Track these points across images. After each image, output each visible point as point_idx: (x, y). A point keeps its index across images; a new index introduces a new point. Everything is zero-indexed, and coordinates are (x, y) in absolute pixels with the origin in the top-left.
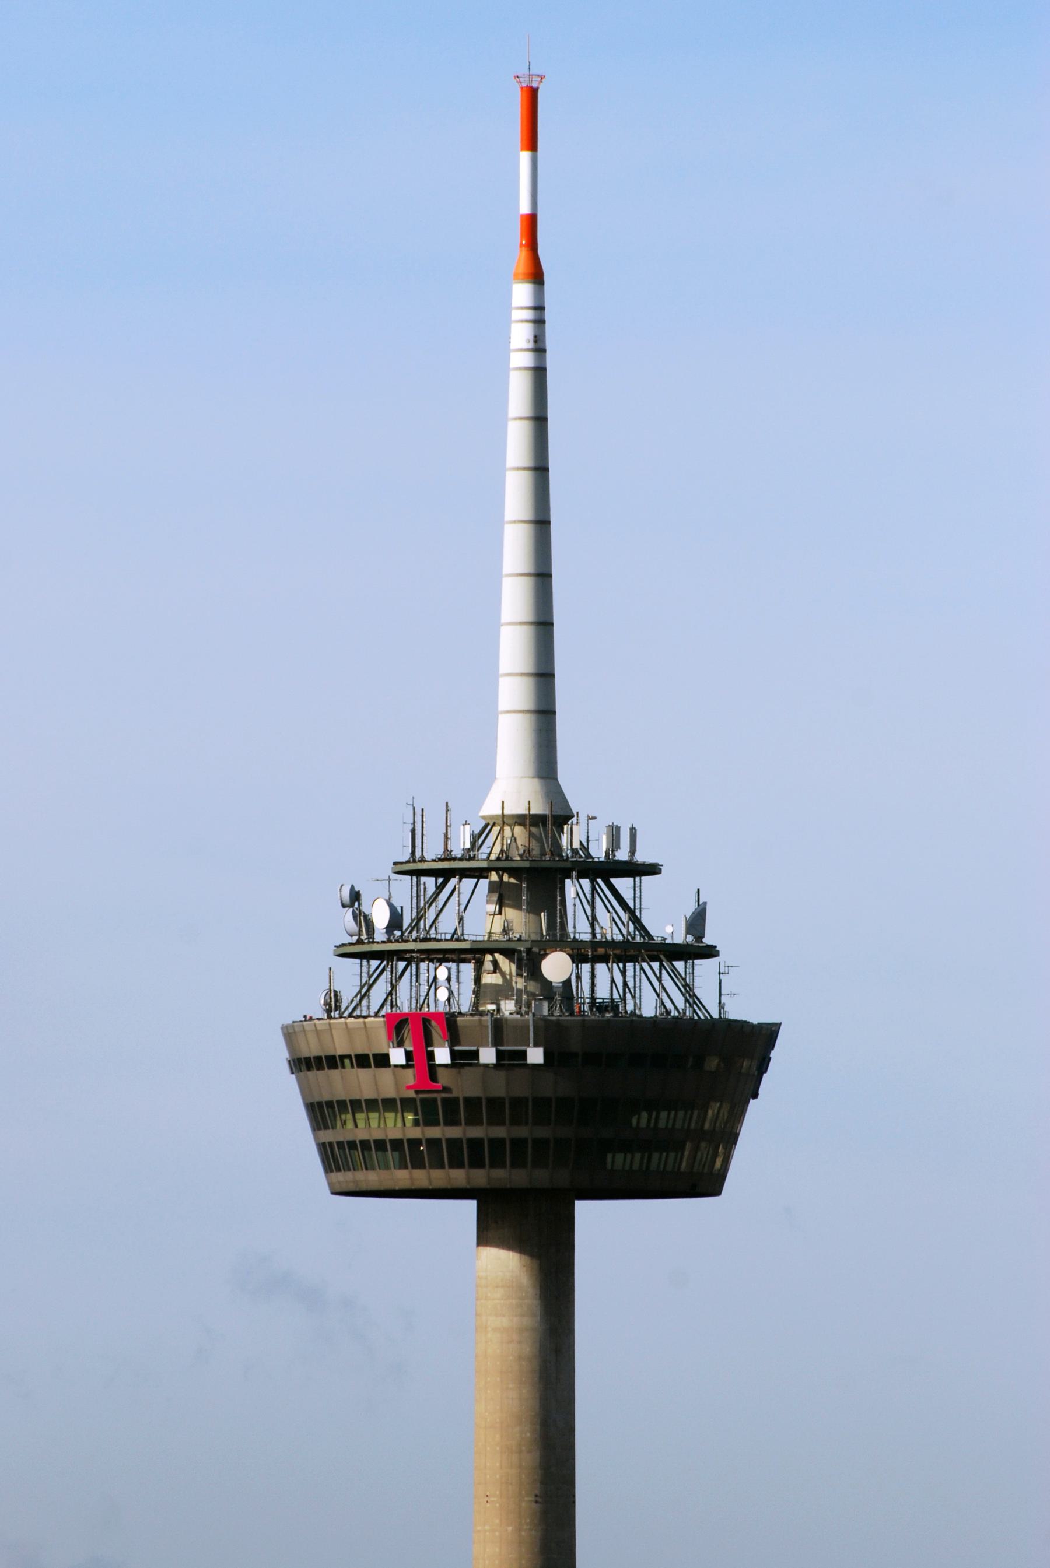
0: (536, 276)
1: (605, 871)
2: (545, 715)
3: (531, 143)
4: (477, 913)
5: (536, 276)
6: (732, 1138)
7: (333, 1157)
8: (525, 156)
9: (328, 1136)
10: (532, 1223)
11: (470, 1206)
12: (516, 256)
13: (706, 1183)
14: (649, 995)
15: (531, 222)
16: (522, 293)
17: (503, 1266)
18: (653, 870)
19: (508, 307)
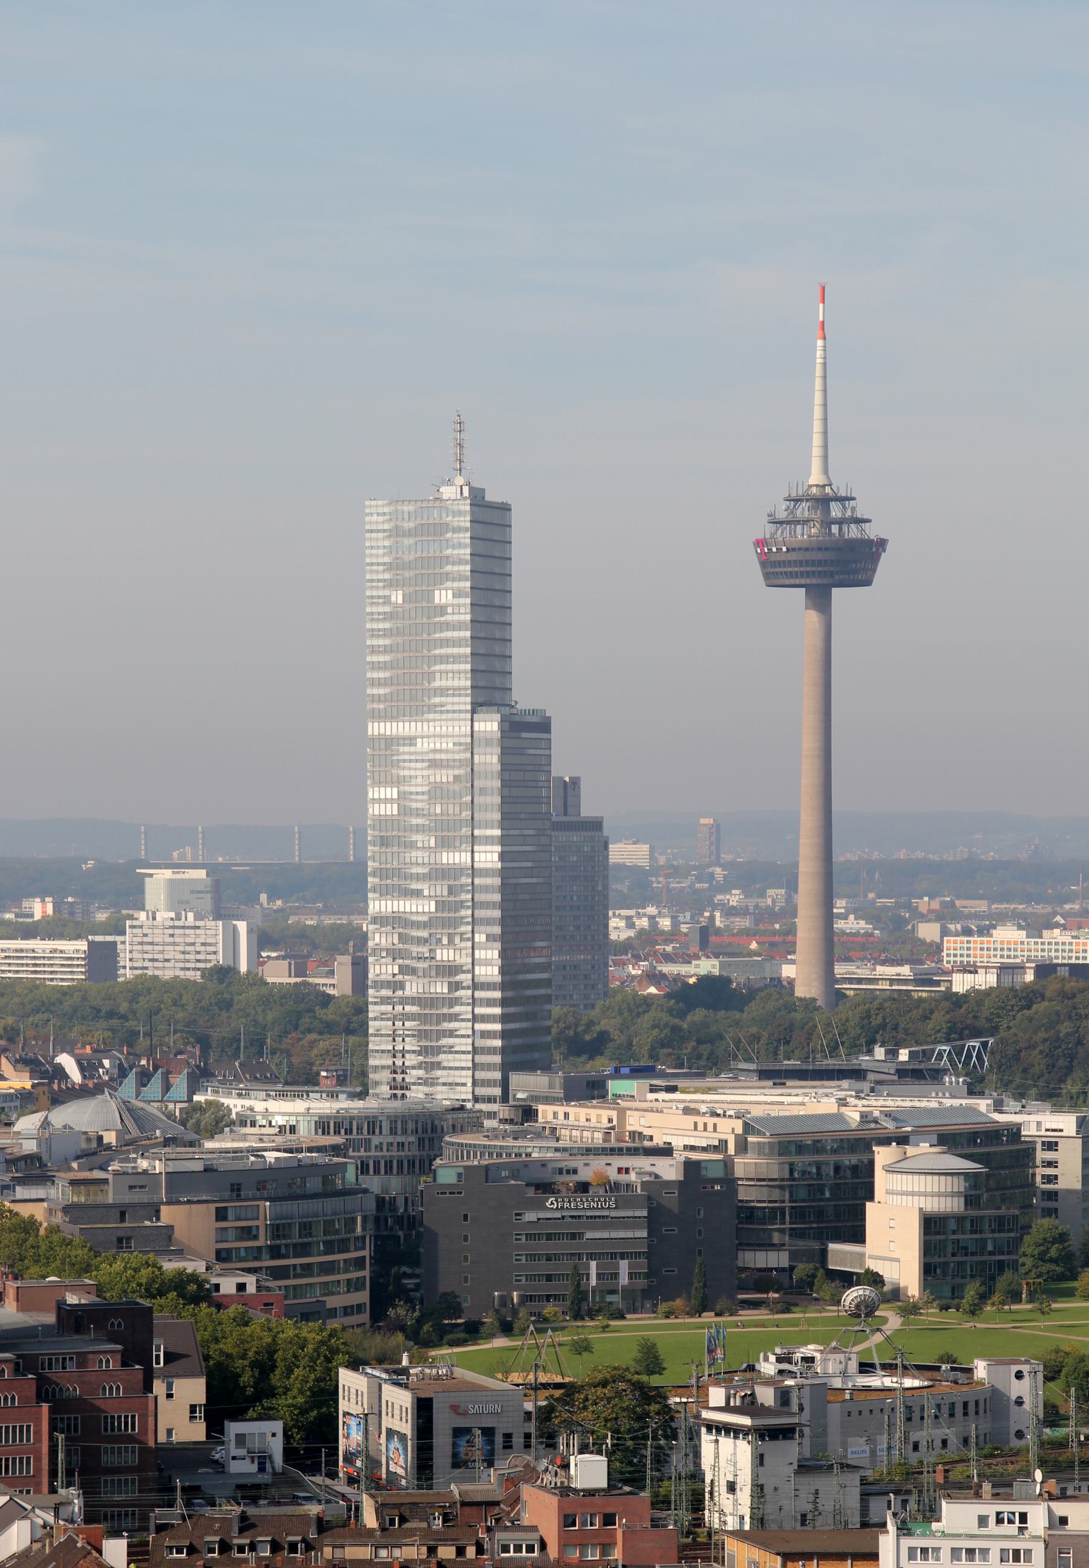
0: (824, 338)
1: (842, 500)
2: (825, 457)
3: (823, 302)
4: (803, 510)
5: (824, 338)
6: (874, 571)
7: (767, 576)
8: (821, 305)
9: (930, 1260)
10: (820, 599)
11: (804, 590)
12: (819, 333)
13: (868, 582)
14: (853, 532)
15: (823, 322)
16: (820, 343)
17: (813, 617)
18: (869, 521)
19: (816, 346)
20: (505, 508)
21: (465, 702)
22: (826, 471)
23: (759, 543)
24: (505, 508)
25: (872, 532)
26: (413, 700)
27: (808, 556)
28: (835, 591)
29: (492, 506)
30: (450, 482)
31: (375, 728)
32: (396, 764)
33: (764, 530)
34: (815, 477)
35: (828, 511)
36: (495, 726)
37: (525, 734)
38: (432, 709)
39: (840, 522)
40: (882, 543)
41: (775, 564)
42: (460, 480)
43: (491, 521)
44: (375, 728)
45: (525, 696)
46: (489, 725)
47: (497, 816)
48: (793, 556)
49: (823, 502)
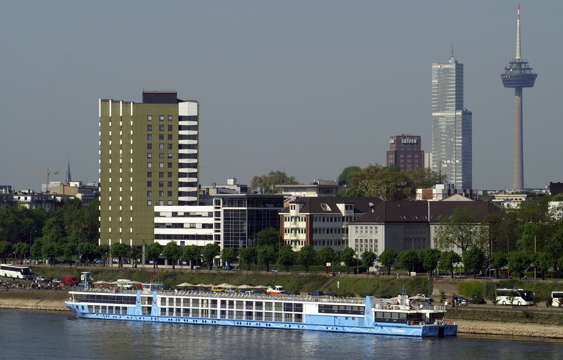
2: (520, 52)
7: (504, 84)
10: (519, 92)
13: (532, 86)
14: (528, 72)
17: (518, 97)
20: (462, 65)
21: (454, 108)
22: (520, 55)
23: (502, 75)
24: (462, 65)
25: (533, 72)
26: (442, 107)
27: (516, 79)
28: (523, 88)
29: (460, 64)
30: (450, 59)
31: (434, 114)
32: (438, 122)
33: (504, 72)
34: (518, 57)
35: (521, 66)
36: (461, 113)
37: (467, 115)
38: (447, 109)
39: (524, 69)
40: (536, 75)
41: (507, 81)
42: (453, 59)
43: (459, 68)
44: (434, 114)
45: (467, 106)
46: (459, 113)
47: (461, 134)
48: (512, 79)
49: (520, 64)
